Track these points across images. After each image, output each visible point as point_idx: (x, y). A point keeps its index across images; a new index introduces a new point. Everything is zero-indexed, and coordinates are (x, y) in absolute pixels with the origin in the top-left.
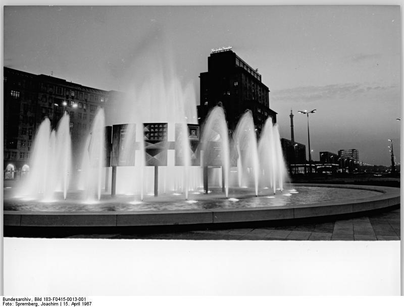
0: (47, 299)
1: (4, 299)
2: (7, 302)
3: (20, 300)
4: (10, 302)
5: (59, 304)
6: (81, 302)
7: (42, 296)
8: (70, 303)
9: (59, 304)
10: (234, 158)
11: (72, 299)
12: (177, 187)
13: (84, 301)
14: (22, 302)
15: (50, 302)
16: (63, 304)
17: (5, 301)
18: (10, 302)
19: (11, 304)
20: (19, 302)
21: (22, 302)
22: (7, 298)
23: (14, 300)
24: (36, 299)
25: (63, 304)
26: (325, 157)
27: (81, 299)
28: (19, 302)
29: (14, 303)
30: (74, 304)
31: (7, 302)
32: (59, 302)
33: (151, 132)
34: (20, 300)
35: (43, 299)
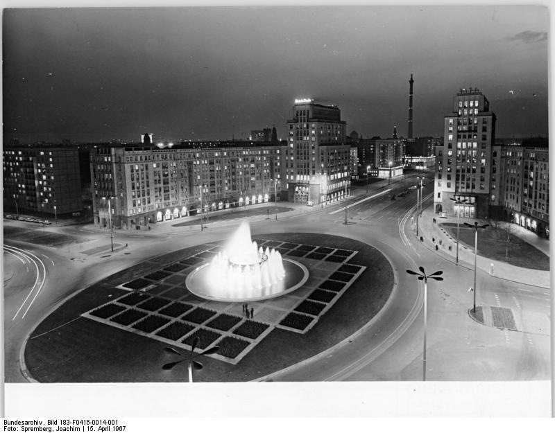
0: (64, 422)
1: (5, 422)
2: (10, 426)
3: (27, 423)
4: (13, 426)
5: (82, 429)
6: (111, 426)
8: (96, 427)
9: (82, 429)
11: (100, 422)
13: (115, 425)
14: (30, 426)
15: (69, 426)
16: (86, 429)
17: (7, 425)
18: (13, 426)
19: (15, 429)
20: (26, 426)
21: (30, 426)
22: (9, 420)
23: (19, 423)
24: (49, 422)
25: (86, 429)
28: (26, 426)
29: (19, 427)
30: (102, 429)
31: (10, 426)
32: (80, 426)
34: (27, 423)
35: (59, 423)
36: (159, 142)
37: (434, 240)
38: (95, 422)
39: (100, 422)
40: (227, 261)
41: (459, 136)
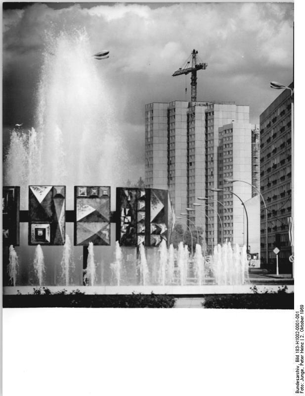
0: (297, 328)
1: (297, 392)
2: (300, 389)
3: (298, 377)
4: (300, 386)
5: (302, 341)
6: (300, 315)
7: (293, 355)
8: (301, 334)
10: (235, 260)
11: (297, 322)
12: (226, 270)
13: (299, 313)
14: (300, 375)
15: (300, 323)
16: (302, 338)
17: (299, 391)
18: (300, 386)
20: (300, 378)
21: (300, 375)
23: (298, 382)
24: (297, 361)
25: (302, 338)
26: (6, 157)
27: (297, 316)
29: (301, 381)
31: (300, 389)
32: (300, 342)
33: (147, 234)
34: (298, 377)
35: (297, 354)
36: (9, 231)
37: (189, 63)
38: (297, 316)
39: (297, 322)
40: (139, 178)
41: (273, 224)
